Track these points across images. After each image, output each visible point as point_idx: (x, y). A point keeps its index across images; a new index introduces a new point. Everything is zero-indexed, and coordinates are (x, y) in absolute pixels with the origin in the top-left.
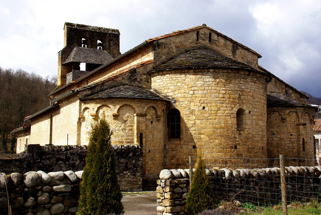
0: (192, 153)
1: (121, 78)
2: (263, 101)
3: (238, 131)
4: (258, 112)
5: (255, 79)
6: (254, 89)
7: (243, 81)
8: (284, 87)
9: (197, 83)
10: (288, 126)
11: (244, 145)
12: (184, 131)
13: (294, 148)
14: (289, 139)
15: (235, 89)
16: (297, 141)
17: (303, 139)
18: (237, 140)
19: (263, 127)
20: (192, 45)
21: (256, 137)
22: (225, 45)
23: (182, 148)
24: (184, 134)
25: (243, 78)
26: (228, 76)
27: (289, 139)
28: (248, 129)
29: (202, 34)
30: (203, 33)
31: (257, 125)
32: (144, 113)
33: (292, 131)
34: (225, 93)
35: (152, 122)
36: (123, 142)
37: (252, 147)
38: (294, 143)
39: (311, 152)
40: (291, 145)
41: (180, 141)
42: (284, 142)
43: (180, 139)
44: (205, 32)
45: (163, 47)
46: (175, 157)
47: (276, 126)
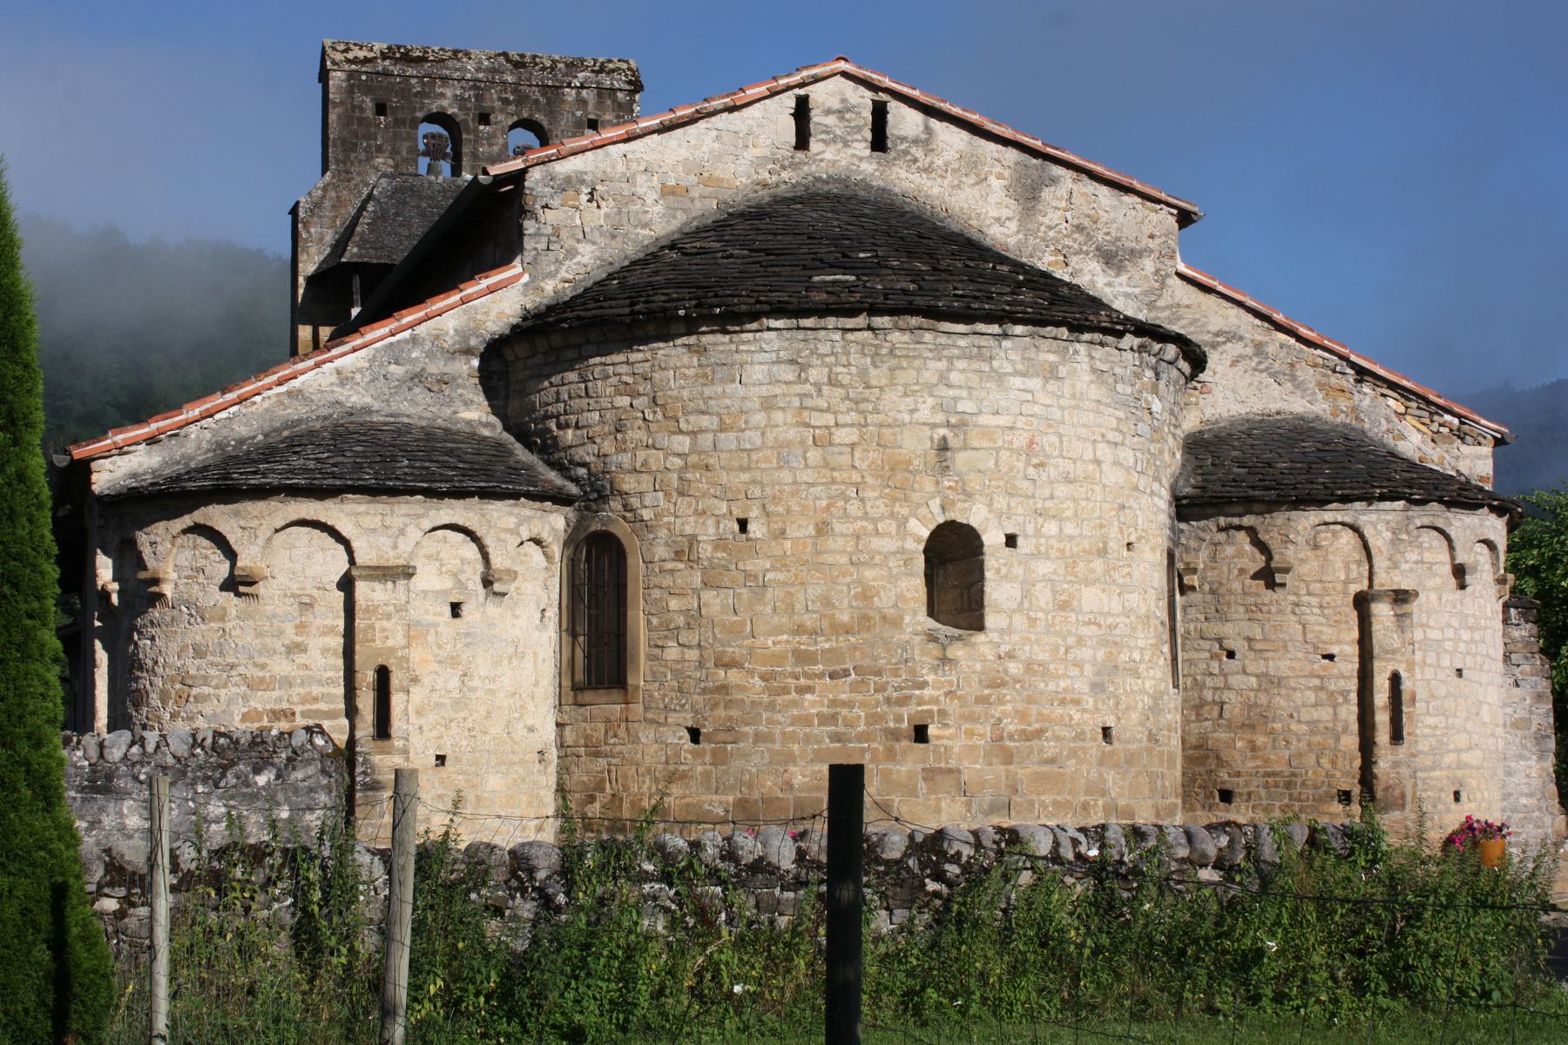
0: (682, 768)
3: (931, 646)
5: (1052, 358)
7: (963, 371)
10: (1309, 605)
14: (1317, 682)
17: (1395, 679)
18: (927, 692)
21: (1058, 677)
23: (637, 740)
25: (971, 358)
26: (876, 346)
27: (1317, 682)
29: (828, 112)
30: (836, 105)
32: (402, 562)
33: (1328, 632)
35: (456, 609)
36: (293, 714)
37: (1023, 732)
39: (1459, 751)
40: (1325, 714)
42: (1288, 698)
43: (626, 693)
44: (844, 101)
46: (603, 790)
47: (1242, 609)
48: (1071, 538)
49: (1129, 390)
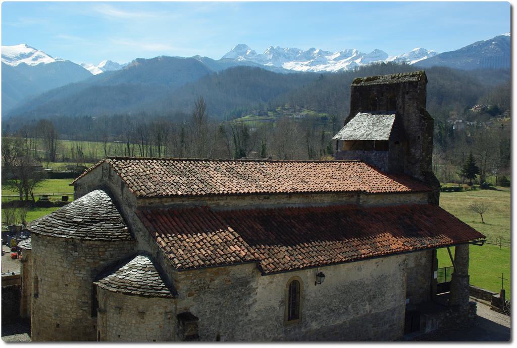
48: (50, 282)
49: (64, 250)
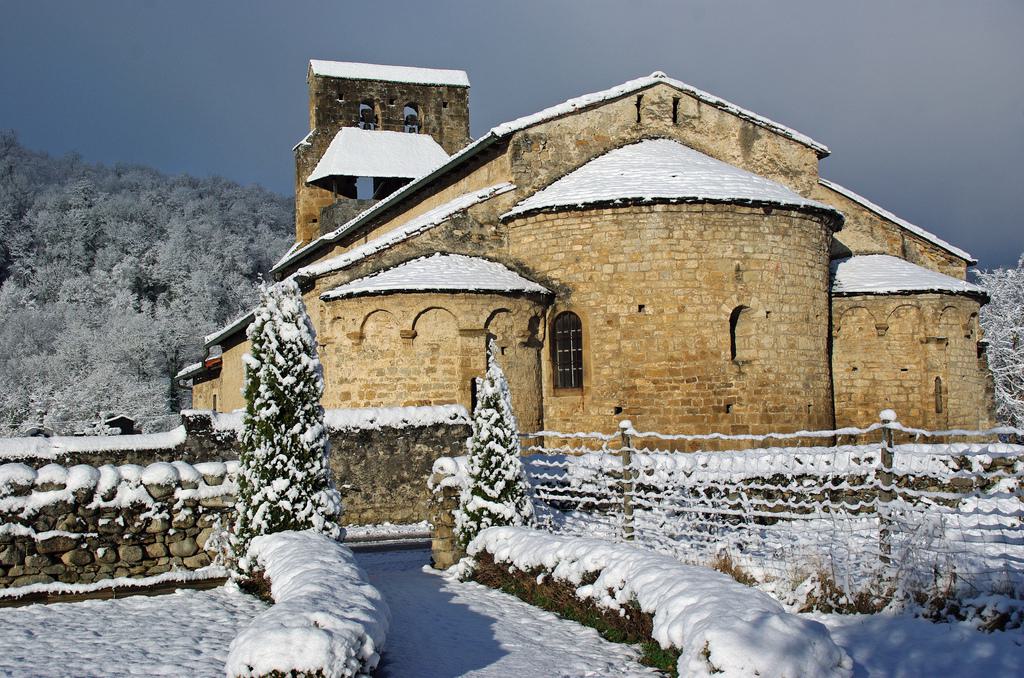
1: (429, 237)
2: (810, 283)
4: (794, 314)
6: (780, 251)
7: (746, 232)
8: (897, 233)
9: (623, 243)
11: (753, 401)
12: (593, 370)
13: (913, 406)
14: (898, 383)
15: (726, 254)
16: (919, 387)
19: (811, 353)
20: (624, 135)
22: (720, 128)
23: (588, 413)
24: (593, 377)
25: (750, 225)
28: (765, 359)
29: (653, 103)
31: (792, 346)
34: (611, 280)
38: (913, 392)
40: (902, 398)
41: (583, 395)
45: (541, 147)
